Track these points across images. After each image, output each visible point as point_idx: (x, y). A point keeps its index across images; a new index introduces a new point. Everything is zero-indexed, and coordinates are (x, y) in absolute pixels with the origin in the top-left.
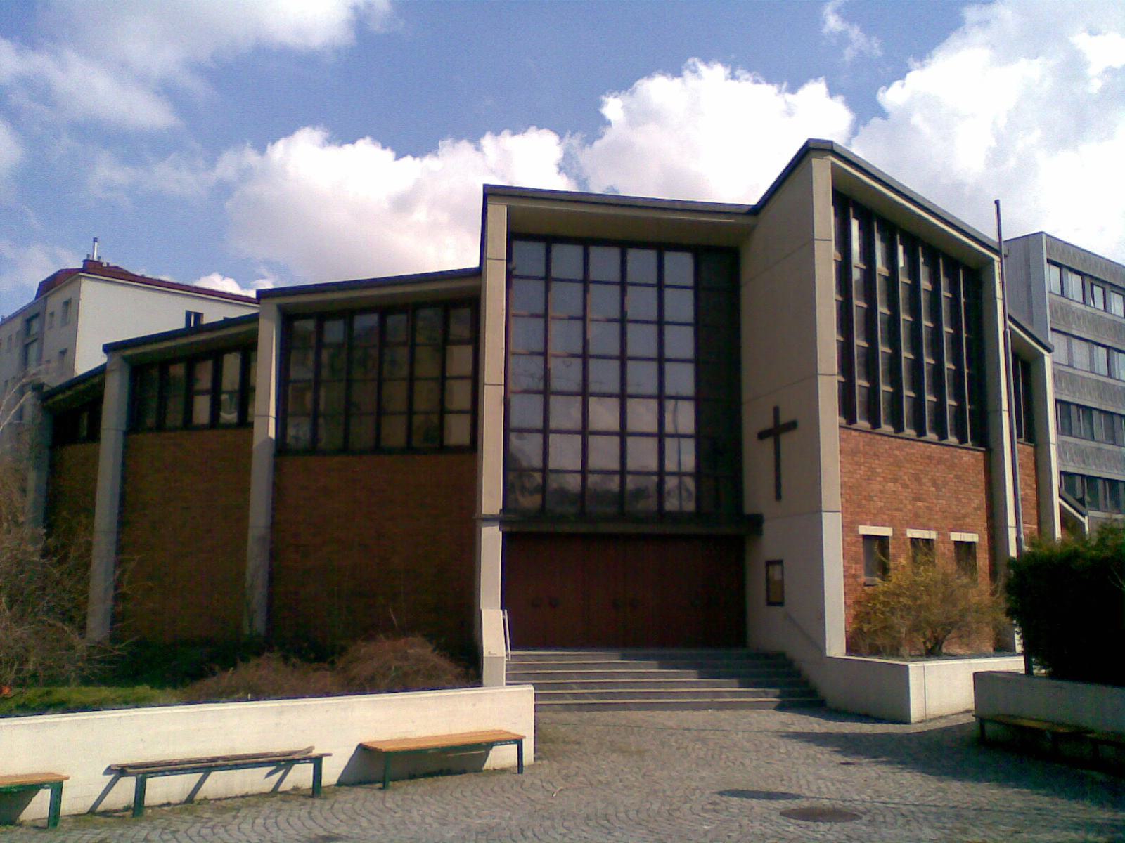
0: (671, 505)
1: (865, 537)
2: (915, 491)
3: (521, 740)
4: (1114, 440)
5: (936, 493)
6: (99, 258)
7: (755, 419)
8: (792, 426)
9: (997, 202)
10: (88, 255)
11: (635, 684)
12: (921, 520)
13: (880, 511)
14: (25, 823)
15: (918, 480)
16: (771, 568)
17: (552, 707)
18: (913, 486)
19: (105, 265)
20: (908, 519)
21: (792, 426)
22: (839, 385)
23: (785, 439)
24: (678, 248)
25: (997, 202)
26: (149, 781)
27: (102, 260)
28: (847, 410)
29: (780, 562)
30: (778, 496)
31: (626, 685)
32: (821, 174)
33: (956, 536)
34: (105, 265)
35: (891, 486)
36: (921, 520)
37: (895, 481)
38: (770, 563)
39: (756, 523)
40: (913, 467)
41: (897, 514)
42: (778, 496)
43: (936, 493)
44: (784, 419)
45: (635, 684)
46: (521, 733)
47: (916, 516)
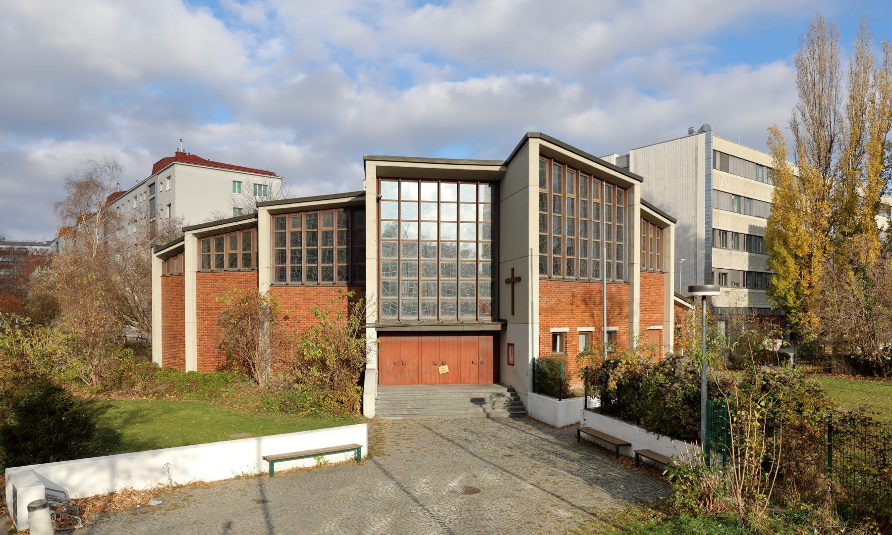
1: (628, 156)
3: (360, 448)
4: (757, 178)
6: (184, 150)
7: (505, 274)
10: (178, 149)
14: (116, 506)
19: (187, 154)
21: (519, 279)
26: (275, 464)
27: (185, 152)
28: (542, 270)
29: (513, 345)
30: (513, 313)
32: (534, 147)
34: (187, 154)
38: (509, 344)
42: (513, 313)
44: (516, 275)
46: (359, 443)
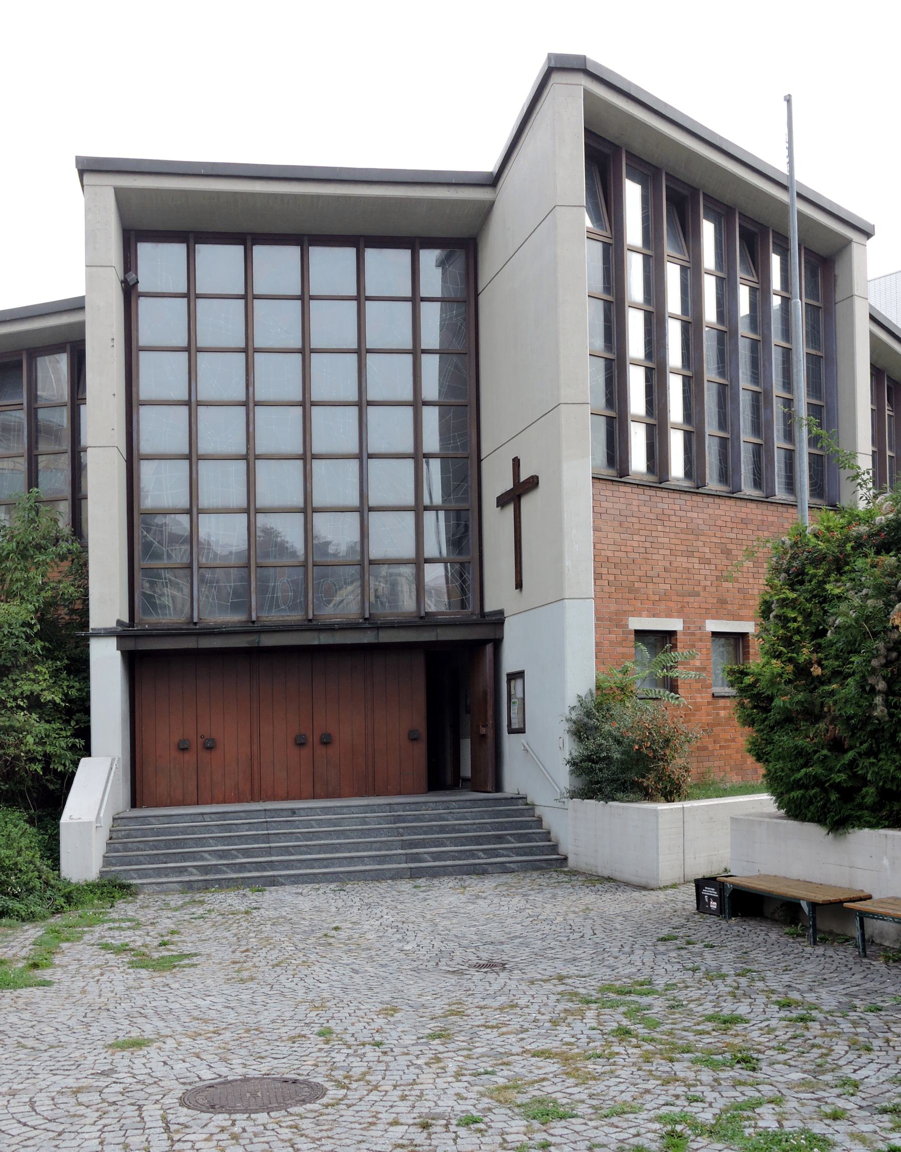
0: (431, 606)
1: (715, 634)
2: (720, 567)
5: (755, 570)
8: (533, 483)
9: (788, 100)
11: (297, 850)
12: (729, 607)
13: (664, 597)
15: (727, 553)
16: (513, 683)
17: (165, 886)
18: (718, 562)
20: (709, 606)
21: (533, 483)
22: (810, 459)
23: (527, 502)
24: (430, 243)
25: (788, 100)
30: (519, 585)
31: (286, 850)
33: (713, 626)
35: (681, 561)
36: (729, 607)
37: (690, 554)
38: (512, 677)
39: (498, 620)
40: (719, 534)
41: (691, 599)
42: (519, 585)
43: (755, 570)
45: (297, 850)
47: (723, 602)
